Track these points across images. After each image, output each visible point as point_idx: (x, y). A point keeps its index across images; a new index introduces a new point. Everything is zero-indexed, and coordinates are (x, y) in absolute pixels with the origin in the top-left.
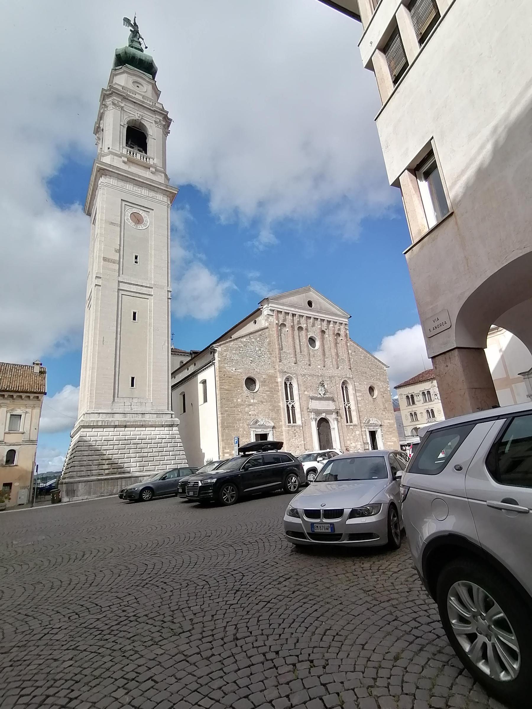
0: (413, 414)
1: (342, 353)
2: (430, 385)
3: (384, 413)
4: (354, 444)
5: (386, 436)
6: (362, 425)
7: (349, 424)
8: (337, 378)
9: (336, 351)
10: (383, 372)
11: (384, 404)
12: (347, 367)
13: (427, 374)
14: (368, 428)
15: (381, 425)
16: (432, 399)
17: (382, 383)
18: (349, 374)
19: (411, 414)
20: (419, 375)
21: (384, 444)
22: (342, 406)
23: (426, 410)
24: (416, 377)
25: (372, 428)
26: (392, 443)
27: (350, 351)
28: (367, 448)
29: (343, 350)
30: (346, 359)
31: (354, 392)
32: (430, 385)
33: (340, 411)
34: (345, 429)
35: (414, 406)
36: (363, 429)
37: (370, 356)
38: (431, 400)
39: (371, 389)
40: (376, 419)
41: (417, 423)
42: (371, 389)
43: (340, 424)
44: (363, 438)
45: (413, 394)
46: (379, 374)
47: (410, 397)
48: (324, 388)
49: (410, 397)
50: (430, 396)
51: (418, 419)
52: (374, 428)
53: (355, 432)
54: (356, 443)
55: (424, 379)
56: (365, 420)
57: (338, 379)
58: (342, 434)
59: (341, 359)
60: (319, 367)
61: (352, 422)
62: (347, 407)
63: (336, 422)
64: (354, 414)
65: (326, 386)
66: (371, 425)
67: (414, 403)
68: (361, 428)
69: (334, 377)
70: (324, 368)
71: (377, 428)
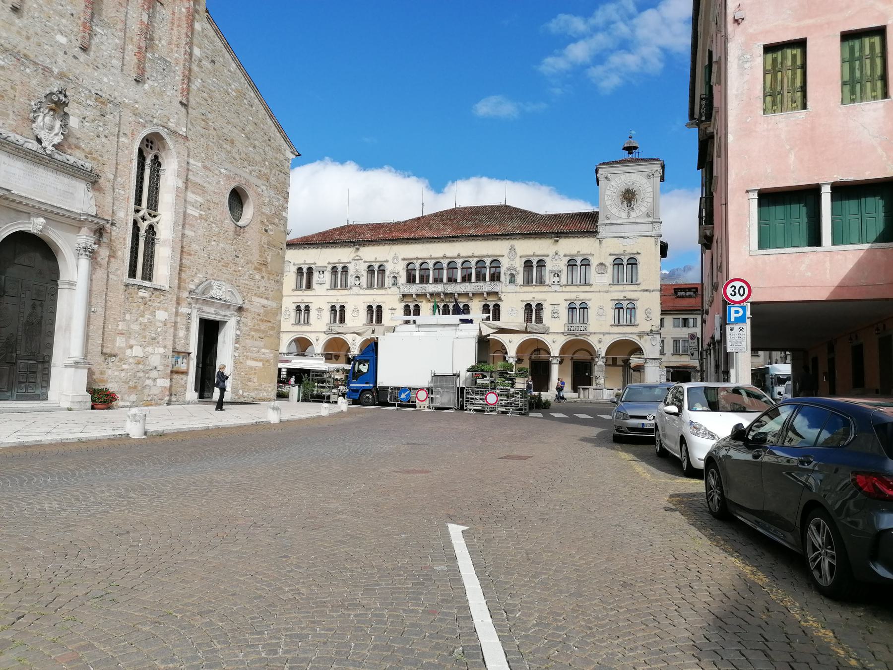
0: (303, 308)
1: (170, 43)
2: (353, 255)
3: (258, 277)
4: (137, 351)
5: (249, 342)
6: (185, 294)
7: (138, 280)
8: (128, 117)
9: (145, 19)
10: (281, 162)
11: (262, 251)
12: (173, 94)
13: (350, 231)
14: (199, 310)
15: (240, 309)
16: (349, 284)
17: (272, 193)
18: (177, 120)
19: (298, 308)
20: (336, 229)
21: (235, 363)
22: (125, 214)
23: (331, 305)
24: (327, 232)
25: (212, 310)
26: (260, 364)
27: (197, 51)
28: (183, 367)
29: (175, 32)
30: (179, 69)
31: (181, 184)
32: (353, 255)
33: (115, 232)
34: (118, 295)
35: (309, 292)
36: (184, 310)
37: (256, 101)
38: (346, 286)
39: (237, 198)
40: (229, 288)
41: (306, 328)
42: (237, 198)
43: (100, 274)
44: (175, 336)
45: (313, 266)
46: (270, 163)
47: (305, 270)
48: (65, 126)
49: (305, 270)
50: (346, 278)
51: (311, 321)
52: (216, 313)
53: (153, 313)
54: (149, 350)
55: (343, 239)
56: (197, 281)
57: (132, 119)
58: (101, 310)
59: (161, 59)
60: (62, 40)
61: (150, 279)
62: (144, 226)
63: (84, 263)
64: (164, 255)
65: (73, 122)
66: (211, 301)
67: (309, 286)
68: (178, 303)
69: (115, 105)
70: (82, 57)
71: (228, 313)
